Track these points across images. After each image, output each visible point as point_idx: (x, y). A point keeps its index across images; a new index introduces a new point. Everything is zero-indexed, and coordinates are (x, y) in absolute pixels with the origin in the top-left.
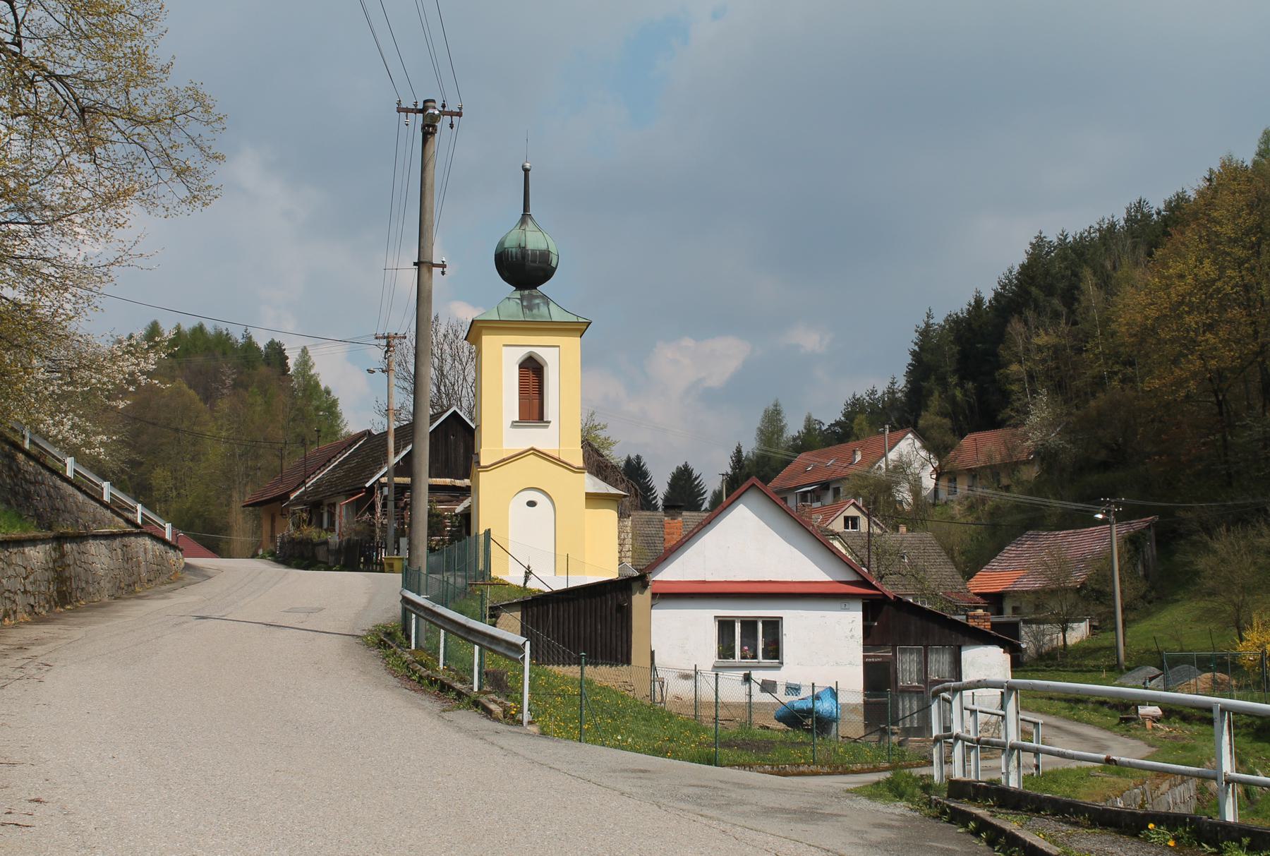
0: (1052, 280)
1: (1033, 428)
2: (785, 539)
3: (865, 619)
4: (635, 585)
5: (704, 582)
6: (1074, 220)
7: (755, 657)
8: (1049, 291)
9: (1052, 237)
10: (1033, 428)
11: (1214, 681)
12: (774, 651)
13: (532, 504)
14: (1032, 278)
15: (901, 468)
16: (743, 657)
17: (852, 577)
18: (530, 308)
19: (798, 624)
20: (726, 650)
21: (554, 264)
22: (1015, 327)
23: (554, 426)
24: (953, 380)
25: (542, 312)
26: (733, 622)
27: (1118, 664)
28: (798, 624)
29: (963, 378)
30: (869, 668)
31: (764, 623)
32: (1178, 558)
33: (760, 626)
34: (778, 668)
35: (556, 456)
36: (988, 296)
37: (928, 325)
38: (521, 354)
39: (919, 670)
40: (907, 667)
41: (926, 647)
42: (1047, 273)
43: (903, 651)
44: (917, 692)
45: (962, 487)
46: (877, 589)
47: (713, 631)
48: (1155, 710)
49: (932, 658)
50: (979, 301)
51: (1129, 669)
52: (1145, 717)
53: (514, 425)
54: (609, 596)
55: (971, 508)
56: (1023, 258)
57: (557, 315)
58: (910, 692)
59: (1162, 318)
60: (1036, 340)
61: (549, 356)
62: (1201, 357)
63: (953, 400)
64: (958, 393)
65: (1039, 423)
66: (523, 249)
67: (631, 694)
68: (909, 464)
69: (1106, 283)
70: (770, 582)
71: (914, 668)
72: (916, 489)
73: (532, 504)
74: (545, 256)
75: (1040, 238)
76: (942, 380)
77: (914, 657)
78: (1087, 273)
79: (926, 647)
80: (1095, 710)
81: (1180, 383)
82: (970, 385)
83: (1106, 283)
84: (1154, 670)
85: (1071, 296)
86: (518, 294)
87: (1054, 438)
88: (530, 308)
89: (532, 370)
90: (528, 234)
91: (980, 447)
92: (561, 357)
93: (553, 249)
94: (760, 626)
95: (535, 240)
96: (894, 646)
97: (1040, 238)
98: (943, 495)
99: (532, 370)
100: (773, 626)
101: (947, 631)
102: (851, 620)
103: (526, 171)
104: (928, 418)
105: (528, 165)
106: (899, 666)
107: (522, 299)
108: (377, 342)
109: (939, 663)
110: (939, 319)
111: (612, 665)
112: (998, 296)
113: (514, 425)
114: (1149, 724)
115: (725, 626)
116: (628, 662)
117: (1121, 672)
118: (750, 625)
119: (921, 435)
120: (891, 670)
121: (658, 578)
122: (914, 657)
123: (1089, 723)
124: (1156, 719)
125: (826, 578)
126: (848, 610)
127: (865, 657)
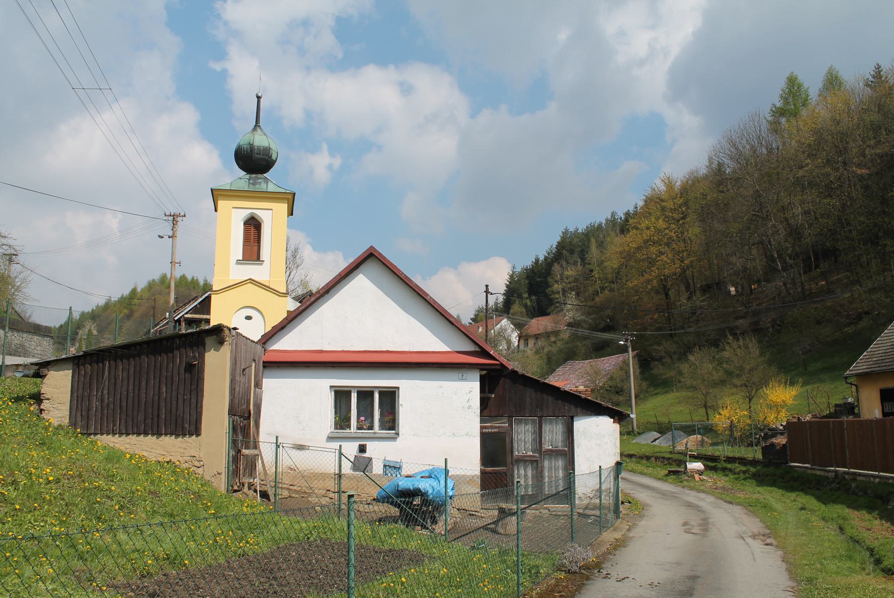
0: (571, 248)
1: (568, 310)
2: (403, 308)
3: (482, 390)
4: (209, 341)
5: (321, 352)
6: (579, 224)
7: (371, 427)
8: (572, 252)
9: (572, 229)
10: (568, 310)
11: (703, 440)
12: (390, 422)
13: (249, 318)
14: (564, 248)
15: (503, 330)
16: (359, 428)
17: (471, 348)
18: (254, 184)
19: (412, 391)
20: (342, 421)
21: (274, 157)
22: (556, 268)
23: (266, 264)
24: (526, 295)
25: (263, 187)
26: (350, 392)
27: (633, 431)
28: (412, 391)
29: (530, 295)
30: (485, 438)
31: (380, 393)
32: (655, 371)
33: (377, 396)
34: (394, 439)
35: (267, 284)
36: (542, 258)
37: (513, 272)
38: (244, 214)
39: (534, 440)
40: (522, 437)
41: (540, 417)
42: (571, 243)
43: (519, 422)
44: (532, 462)
45: (531, 342)
46: (495, 359)
47: (328, 401)
48: (698, 465)
49: (546, 428)
50: (537, 260)
51: (639, 434)
52: (693, 471)
53: (238, 262)
54: (177, 353)
55: (537, 352)
56: (559, 239)
57: (271, 188)
58: (525, 461)
59: (638, 249)
60: (566, 273)
61: (265, 217)
62: (658, 269)
63: (526, 306)
64: (529, 303)
65: (571, 310)
66: (251, 145)
67: (200, 471)
68: (506, 330)
69: (601, 245)
70: (388, 352)
71: (529, 438)
72: (509, 342)
73: (249, 318)
74: (267, 151)
75: (566, 230)
76: (520, 296)
77: (529, 427)
78: (593, 240)
79: (540, 417)
80: (639, 463)
81: (649, 281)
82: (534, 298)
83: (601, 245)
84: (656, 435)
85: (583, 254)
86: (248, 176)
87: (579, 317)
88: (254, 184)
89: (253, 226)
90: (256, 136)
91: (540, 324)
92: (273, 216)
93: (273, 146)
94: (377, 396)
95: (260, 141)
96: (510, 417)
97: (566, 230)
98: (522, 347)
99: (253, 226)
100: (390, 397)
101: (560, 402)
102: (468, 390)
103: (259, 98)
104: (516, 308)
105: (260, 95)
106: (515, 437)
107: (249, 180)
108: (166, 218)
109: (553, 433)
110: (518, 269)
111: (177, 436)
112: (546, 259)
113: (238, 262)
114: (697, 476)
115: (341, 396)
116: (197, 432)
117: (635, 435)
118: (365, 395)
119: (509, 318)
120: (507, 440)
121: (276, 347)
122: (529, 427)
123: (642, 473)
124: (701, 473)
125: (444, 348)
126: (466, 380)
127: (482, 428)
